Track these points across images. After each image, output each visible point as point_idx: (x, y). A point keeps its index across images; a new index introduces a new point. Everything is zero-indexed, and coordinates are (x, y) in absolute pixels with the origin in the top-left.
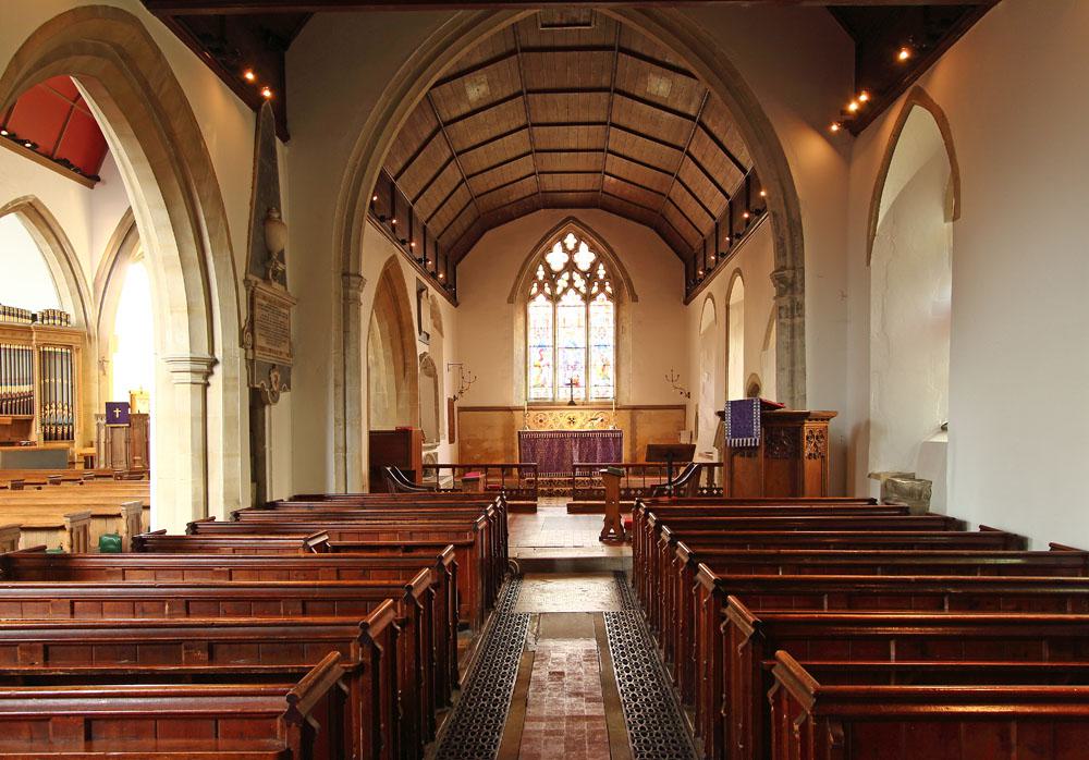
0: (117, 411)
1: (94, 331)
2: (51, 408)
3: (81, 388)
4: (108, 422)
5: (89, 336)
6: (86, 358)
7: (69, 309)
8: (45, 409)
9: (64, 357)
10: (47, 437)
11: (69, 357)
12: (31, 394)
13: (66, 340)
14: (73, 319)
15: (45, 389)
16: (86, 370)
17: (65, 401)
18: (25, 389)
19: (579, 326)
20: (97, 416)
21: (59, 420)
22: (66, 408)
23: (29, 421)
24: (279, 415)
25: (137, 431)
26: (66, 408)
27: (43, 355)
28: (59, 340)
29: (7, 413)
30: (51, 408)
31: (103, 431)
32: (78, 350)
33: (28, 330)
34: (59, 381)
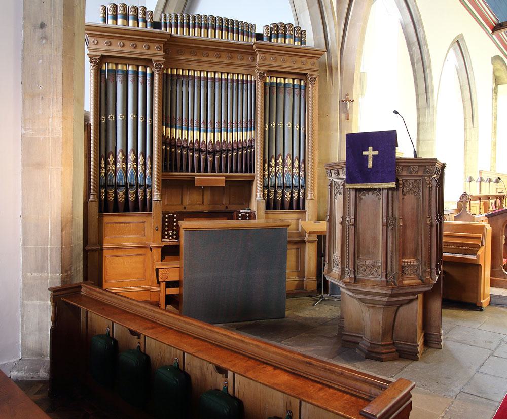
0: (370, 153)
1: (336, 59)
2: (276, 164)
3: (316, 137)
4: (350, 179)
5: (330, 67)
6: (324, 98)
7: (306, 25)
8: (269, 166)
9: (297, 91)
10: (271, 205)
11: (303, 91)
12: (250, 145)
13: (298, 65)
14: (310, 41)
15: (269, 137)
16: (324, 114)
17: (296, 154)
18: (243, 136)
19: (157, 230)
20: (331, 167)
21: (288, 182)
22: (296, 163)
23: (250, 183)
24: (274, 183)
25: (410, 199)
26: (296, 163)
27: (271, 91)
28: (289, 64)
29: (220, 171)
30: (276, 164)
31: (339, 198)
32: (313, 79)
33: (249, 51)
34: (289, 125)
